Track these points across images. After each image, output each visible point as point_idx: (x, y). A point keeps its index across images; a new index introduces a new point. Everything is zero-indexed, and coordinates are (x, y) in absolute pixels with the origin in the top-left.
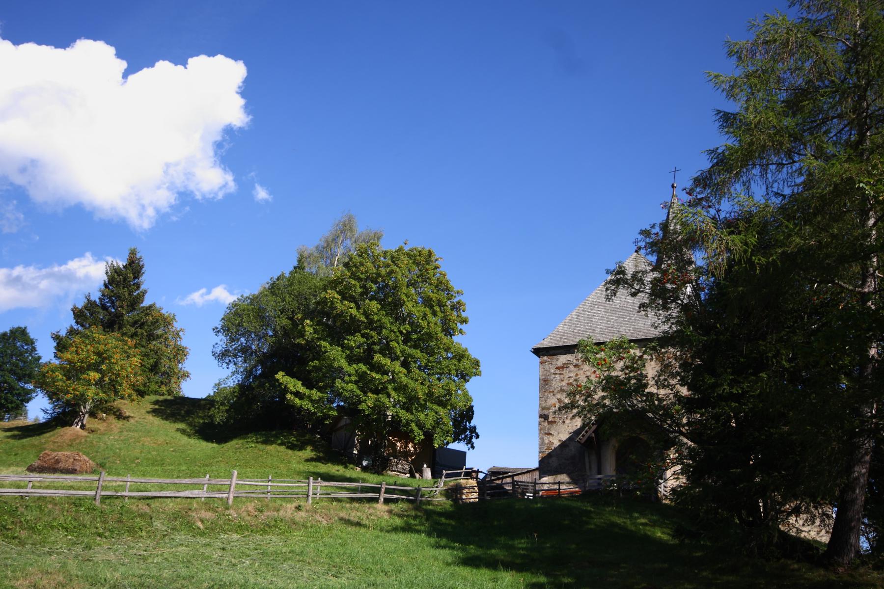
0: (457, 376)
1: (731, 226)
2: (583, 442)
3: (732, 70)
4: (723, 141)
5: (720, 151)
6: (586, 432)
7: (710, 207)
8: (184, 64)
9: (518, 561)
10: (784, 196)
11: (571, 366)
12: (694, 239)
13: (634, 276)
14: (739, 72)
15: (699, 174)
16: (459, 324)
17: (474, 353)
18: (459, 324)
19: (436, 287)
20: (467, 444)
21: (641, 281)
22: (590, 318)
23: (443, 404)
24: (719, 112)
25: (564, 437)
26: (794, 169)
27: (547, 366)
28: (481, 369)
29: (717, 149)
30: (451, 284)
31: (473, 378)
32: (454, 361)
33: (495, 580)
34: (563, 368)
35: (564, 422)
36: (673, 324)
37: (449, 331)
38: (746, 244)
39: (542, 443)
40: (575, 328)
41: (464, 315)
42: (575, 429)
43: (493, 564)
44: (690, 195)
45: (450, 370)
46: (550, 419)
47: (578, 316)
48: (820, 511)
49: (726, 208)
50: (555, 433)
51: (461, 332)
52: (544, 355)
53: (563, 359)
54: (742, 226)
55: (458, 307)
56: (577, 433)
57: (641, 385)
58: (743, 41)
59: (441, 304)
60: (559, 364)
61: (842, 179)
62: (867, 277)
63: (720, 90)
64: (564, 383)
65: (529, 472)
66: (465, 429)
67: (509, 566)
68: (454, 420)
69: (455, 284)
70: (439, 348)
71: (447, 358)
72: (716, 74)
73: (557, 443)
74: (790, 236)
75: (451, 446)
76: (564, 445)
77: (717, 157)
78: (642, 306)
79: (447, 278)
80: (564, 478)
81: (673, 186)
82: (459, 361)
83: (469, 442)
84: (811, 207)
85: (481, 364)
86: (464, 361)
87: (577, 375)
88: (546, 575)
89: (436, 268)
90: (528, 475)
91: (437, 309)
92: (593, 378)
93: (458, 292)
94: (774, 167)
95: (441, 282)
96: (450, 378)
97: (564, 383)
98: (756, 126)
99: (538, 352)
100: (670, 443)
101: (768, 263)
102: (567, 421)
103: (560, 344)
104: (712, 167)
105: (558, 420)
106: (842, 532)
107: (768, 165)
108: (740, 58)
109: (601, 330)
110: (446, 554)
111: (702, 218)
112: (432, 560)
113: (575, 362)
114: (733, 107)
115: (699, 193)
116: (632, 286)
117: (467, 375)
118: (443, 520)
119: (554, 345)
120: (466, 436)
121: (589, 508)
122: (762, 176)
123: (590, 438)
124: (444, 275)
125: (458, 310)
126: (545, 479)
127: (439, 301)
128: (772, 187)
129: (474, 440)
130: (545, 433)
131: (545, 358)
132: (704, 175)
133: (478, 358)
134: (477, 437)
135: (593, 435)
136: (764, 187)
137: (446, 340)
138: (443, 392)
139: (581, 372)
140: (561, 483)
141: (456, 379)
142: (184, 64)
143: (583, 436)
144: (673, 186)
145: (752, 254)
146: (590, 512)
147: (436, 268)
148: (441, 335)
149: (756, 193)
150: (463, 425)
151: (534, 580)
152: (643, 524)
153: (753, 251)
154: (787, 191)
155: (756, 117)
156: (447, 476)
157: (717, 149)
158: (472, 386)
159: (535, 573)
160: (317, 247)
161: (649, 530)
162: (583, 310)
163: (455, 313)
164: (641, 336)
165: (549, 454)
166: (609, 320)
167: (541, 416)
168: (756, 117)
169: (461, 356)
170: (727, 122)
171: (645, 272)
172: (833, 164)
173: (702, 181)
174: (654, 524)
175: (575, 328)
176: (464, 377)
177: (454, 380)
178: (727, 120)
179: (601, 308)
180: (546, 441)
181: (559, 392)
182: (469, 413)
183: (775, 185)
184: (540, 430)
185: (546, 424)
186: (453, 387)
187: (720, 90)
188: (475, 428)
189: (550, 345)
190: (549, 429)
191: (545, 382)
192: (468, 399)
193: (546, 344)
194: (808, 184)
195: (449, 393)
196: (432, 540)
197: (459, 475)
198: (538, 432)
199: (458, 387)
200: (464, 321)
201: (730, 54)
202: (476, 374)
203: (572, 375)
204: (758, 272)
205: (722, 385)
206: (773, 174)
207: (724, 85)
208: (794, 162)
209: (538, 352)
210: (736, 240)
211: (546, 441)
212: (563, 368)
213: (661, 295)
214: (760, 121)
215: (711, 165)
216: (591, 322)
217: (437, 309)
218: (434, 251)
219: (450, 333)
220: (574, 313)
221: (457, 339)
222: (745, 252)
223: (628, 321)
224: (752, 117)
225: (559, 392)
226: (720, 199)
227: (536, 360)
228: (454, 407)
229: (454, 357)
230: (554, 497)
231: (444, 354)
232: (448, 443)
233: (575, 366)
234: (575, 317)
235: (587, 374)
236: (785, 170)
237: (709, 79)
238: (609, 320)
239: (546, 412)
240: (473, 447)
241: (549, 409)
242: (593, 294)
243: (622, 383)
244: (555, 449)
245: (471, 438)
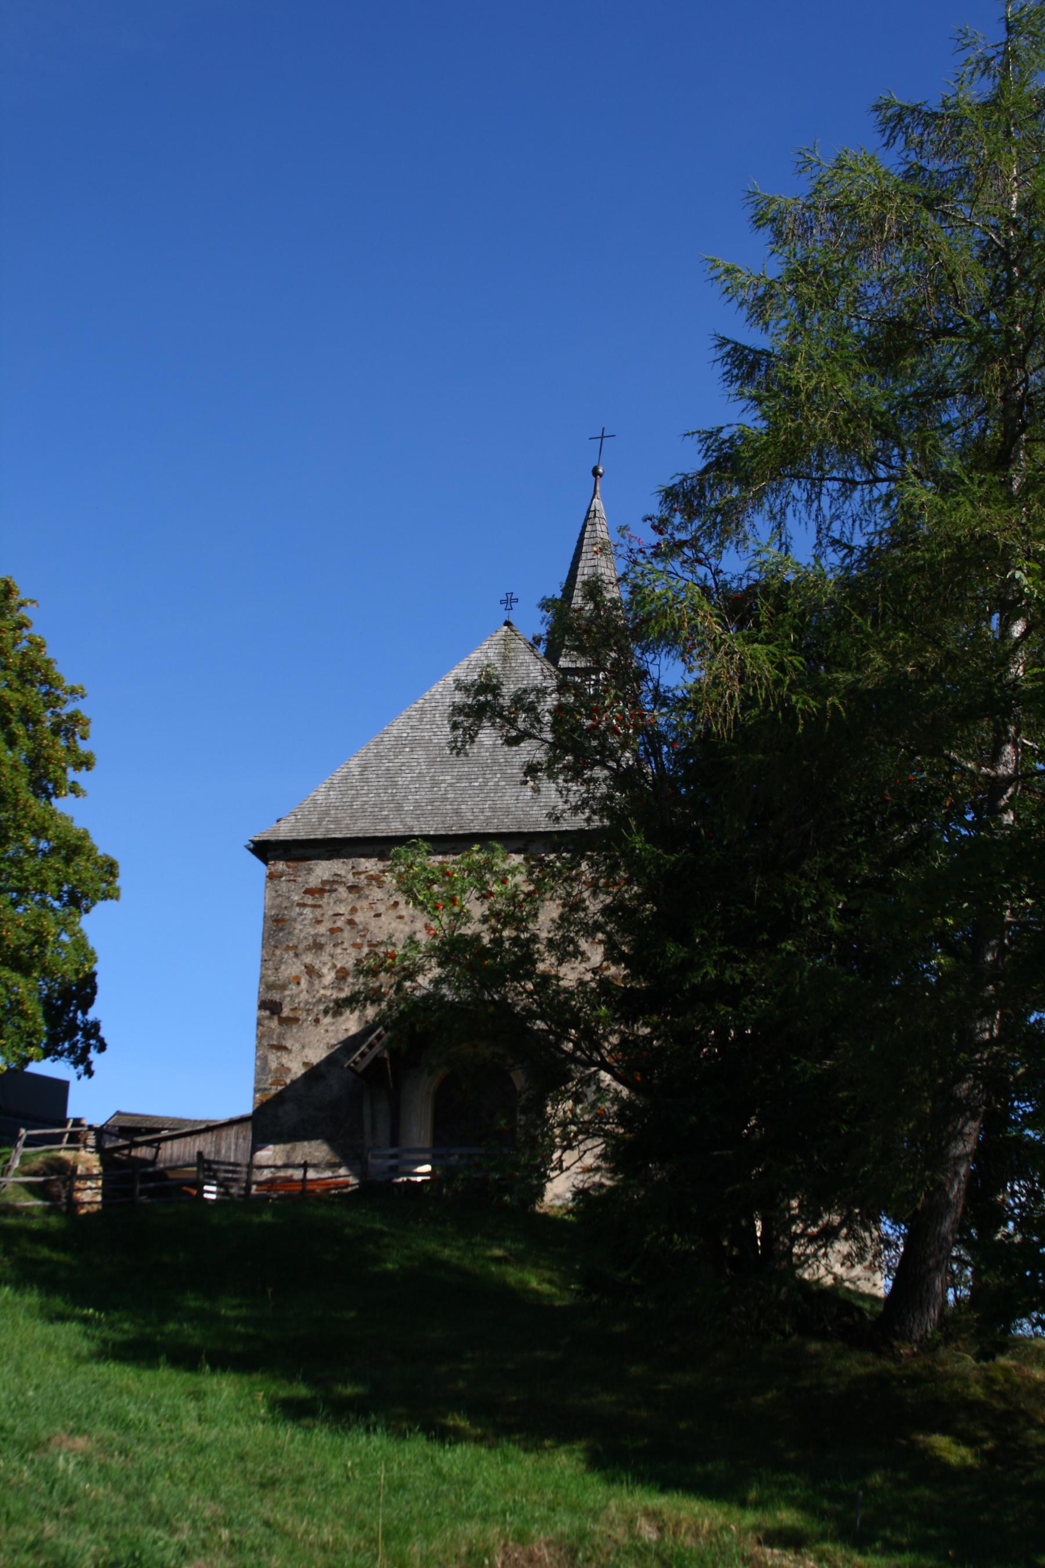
0: (59, 898)
1: (738, 607)
2: (360, 1069)
3: (763, 261)
4: (738, 415)
5: (725, 435)
6: (371, 1046)
7: (699, 561)
9: (239, 1348)
10: (851, 550)
11: (342, 891)
12: (647, 625)
13: (518, 699)
14: (775, 269)
15: (677, 480)
16: (70, 770)
17: (104, 845)
18: (70, 770)
19: (20, 675)
20: (75, 1064)
21: (531, 709)
22: (390, 776)
23: (23, 967)
24: (724, 342)
25: (316, 1055)
26: (876, 494)
27: (283, 886)
28: (119, 882)
29: (720, 430)
30: (58, 669)
31: (101, 904)
32: (56, 862)
33: (197, 1395)
34: (321, 891)
35: (317, 1021)
36: (594, 812)
37: (44, 782)
38: (781, 667)
39: (262, 1068)
40: (355, 798)
41: (83, 747)
42: (342, 1036)
43: (185, 1359)
44: (661, 533)
45: (44, 883)
46: (286, 1012)
47: (364, 768)
48: (875, 1234)
49: (735, 565)
50: (296, 1048)
51: (74, 789)
52: (278, 858)
53: (323, 870)
54: (764, 609)
55: (70, 727)
56: (350, 1044)
57: (526, 959)
58: (789, 195)
59: (28, 718)
60: (314, 882)
61: (973, 536)
62: (1004, 743)
63: (735, 303)
64: (322, 929)
65: (211, 1128)
66: (73, 1028)
67: (224, 1361)
68: (46, 1002)
69: (67, 670)
70: (19, 827)
71: (37, 851)
72: (728, 264)
73: (297, 1070)
74: (865, 648)
75: (33, 1068)
76: (314, 1074)
77: (719, 449)
78: (531, 770)
79: (49, 653)
80: (317, 1150)
81: (595, 473)
82: (68, 860)
83: (82, 1060)
84: (906, 584)
85: (122, 870)
86: (80, 861)
87: (354, 910)
88: (309, 1380)
89: (21, 625)
90: (208, 1136)
91: (19, 729)
92: (422, 937)
93: (73, 691)
94: (836, 485)
95: (32, 663)
96: (43, 904)
97: (322, 929)
98: (808, 397)
99: (263, 850)
100: (552, 1077)
101: (822, 710)
103: (319, 835)
104: (706, 470)
105: (302, 1015)
106: (910, 1279)
107: (822, 479)
108: (778, 234)
109: (417, 805)
110: (69, 1333)
111: (674, 582)
112: (42, 1352)
113: (351, 879)
114: (755, 339)
115: (678, 529)
116: (512, 722)
117: (85, 896)
118: (45, 1252)
119: (302, 836)
120: (73, 1046)
121: (378, 1226)
122: (809, 501)
123: (378, 1061)
124: (40, 646)
125: (70, 734)
126: (267, 1154)
127: (24, 710)
128: (828, 529)
129: (93, 1055)
130: (271, 1044)
131: (281, 866)
132: (687, 485)
133: (115, 856)
134: (102, 1047)
135: (386, 1055)
136: (813, 527)
137: (37, 806)
138: (27, 938)
139: (365, 904)
140: (308, 1161)
141: (56, 904)
143: (363, 1055)
144: (595, 473)
145: (792, 688)
146: (382, 1234)
147: (21, 625)
148: (25, 795)
149: (799, 538)
150: (69, 1019)
151: (283, 1394)
152: (498, 1260)
153: (792, 682)
154: (859, 541)
155: (808, 378)
156: (30, 1142)
157: (720, 430)
158: (97, 924)
159: (291, 1378)
161: (513, 1275)
162: (378, 755)
163: (62, 742)
164: (508, 825)
165: (279, 1096)
166: (435, 783)
167: (263, 1005)
168: (808, 378)
169: (73, 848)
170: (740, 367)
171: (542, 692)
172: (958, 504)
173: (683, 498)
174: (518, 1259)
175: (355, 798)
176: (78, 900)
177: (53, 910)
178: (744, 364)
179: (420, 753)
180: (274, 1065)
181: (309, 948)
182: (84, 990)
183: (836, 525)
184: (260, 1038)
185: (274, 1024)
186: (49, 924)
187: (735, 303)
188: (96, 1025)
189: (294, 836)
190: (281, 1036)
191: (277, 925)
192: (84, 953)
193: (285, 831)
194: (902, 534)
195: (40, 938)
196: (33, 1298)
197: (57, 1139)
198: (253, 1042)
199: (64, 925)
200: (85, 763)
201: (759, 221)
202: (106, 896)
203: (342, 909)
204: (800, 729)
205: (702, 966)
206: (833, 500)
207: (742, 293)
208: (877, 480)
209: (263, 850)
210: (760, 656)
211: (274, 1065)
212: (321, 891)
213: (573, 746)
214: (816, 390)
215: (704, 463)
216: (395, 785)
217: (19, 729)
218: (17, 582)
219: (45, 790)
220: (355, 761)
221: (63, 804)
222: (778, 683)
223: (481, 788)
224: (801, 377)
225: (309, 948)
226: (721, 544)
227: (258, 869)
228: (47, 972)
229: (54, 851)
230: (296, 1198)
231: (31, 841)
232: (27, 1061)
233: (353, 888)
234: (356, 771)
235: (398, 924)
236: (857, 495)
237: (713, 274)
238: (435, 783)
239: (276, 996)
240: (89, 1072)
241: (283, 987)
242: (402, 719)
243: (484, 953)
244: (293, 1082)
245: (86, 1050)
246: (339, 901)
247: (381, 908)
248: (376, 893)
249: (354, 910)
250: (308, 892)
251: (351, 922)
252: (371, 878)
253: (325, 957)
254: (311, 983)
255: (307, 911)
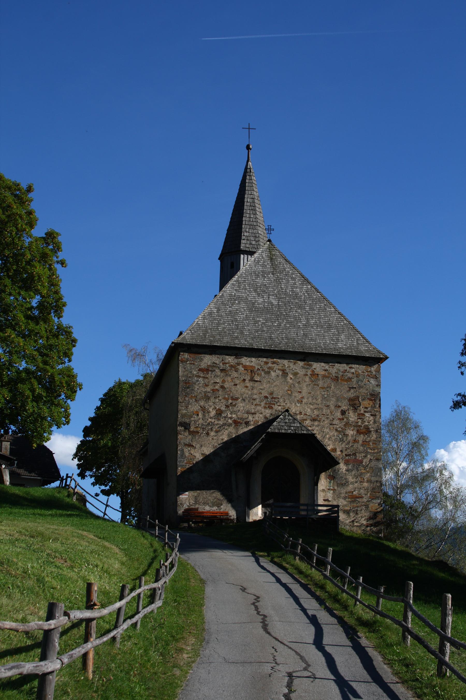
8: (219, 259)
25: (208, 450)
35: (208, 434)
40: (218, 324)
46: (192, 429)
50: (198, 446)
60: (203, 365)
64: (208, 389)
73: (199, 457)
76: (207, 459)
81: (248, 148)
87: (224, 381)
102: (212, 434)
113: (222, 366)
139: (229, 379)
142: (219, 259)
160: (72, 333)
165: (190, 469)
166: (257, 322)
175: (218, 324)
180: (187, 454)
181: (202, 398)
216: (236, 320)
233: (222, 370)
246: (216, 376)
247: (237, 382)
248: (235, 374)
249: (224, 381)
250: (200, 370)
251: (222, 387)
252: (231, 366)
253: (211, 404)
254: (204, 415)
255: (200, 379)
